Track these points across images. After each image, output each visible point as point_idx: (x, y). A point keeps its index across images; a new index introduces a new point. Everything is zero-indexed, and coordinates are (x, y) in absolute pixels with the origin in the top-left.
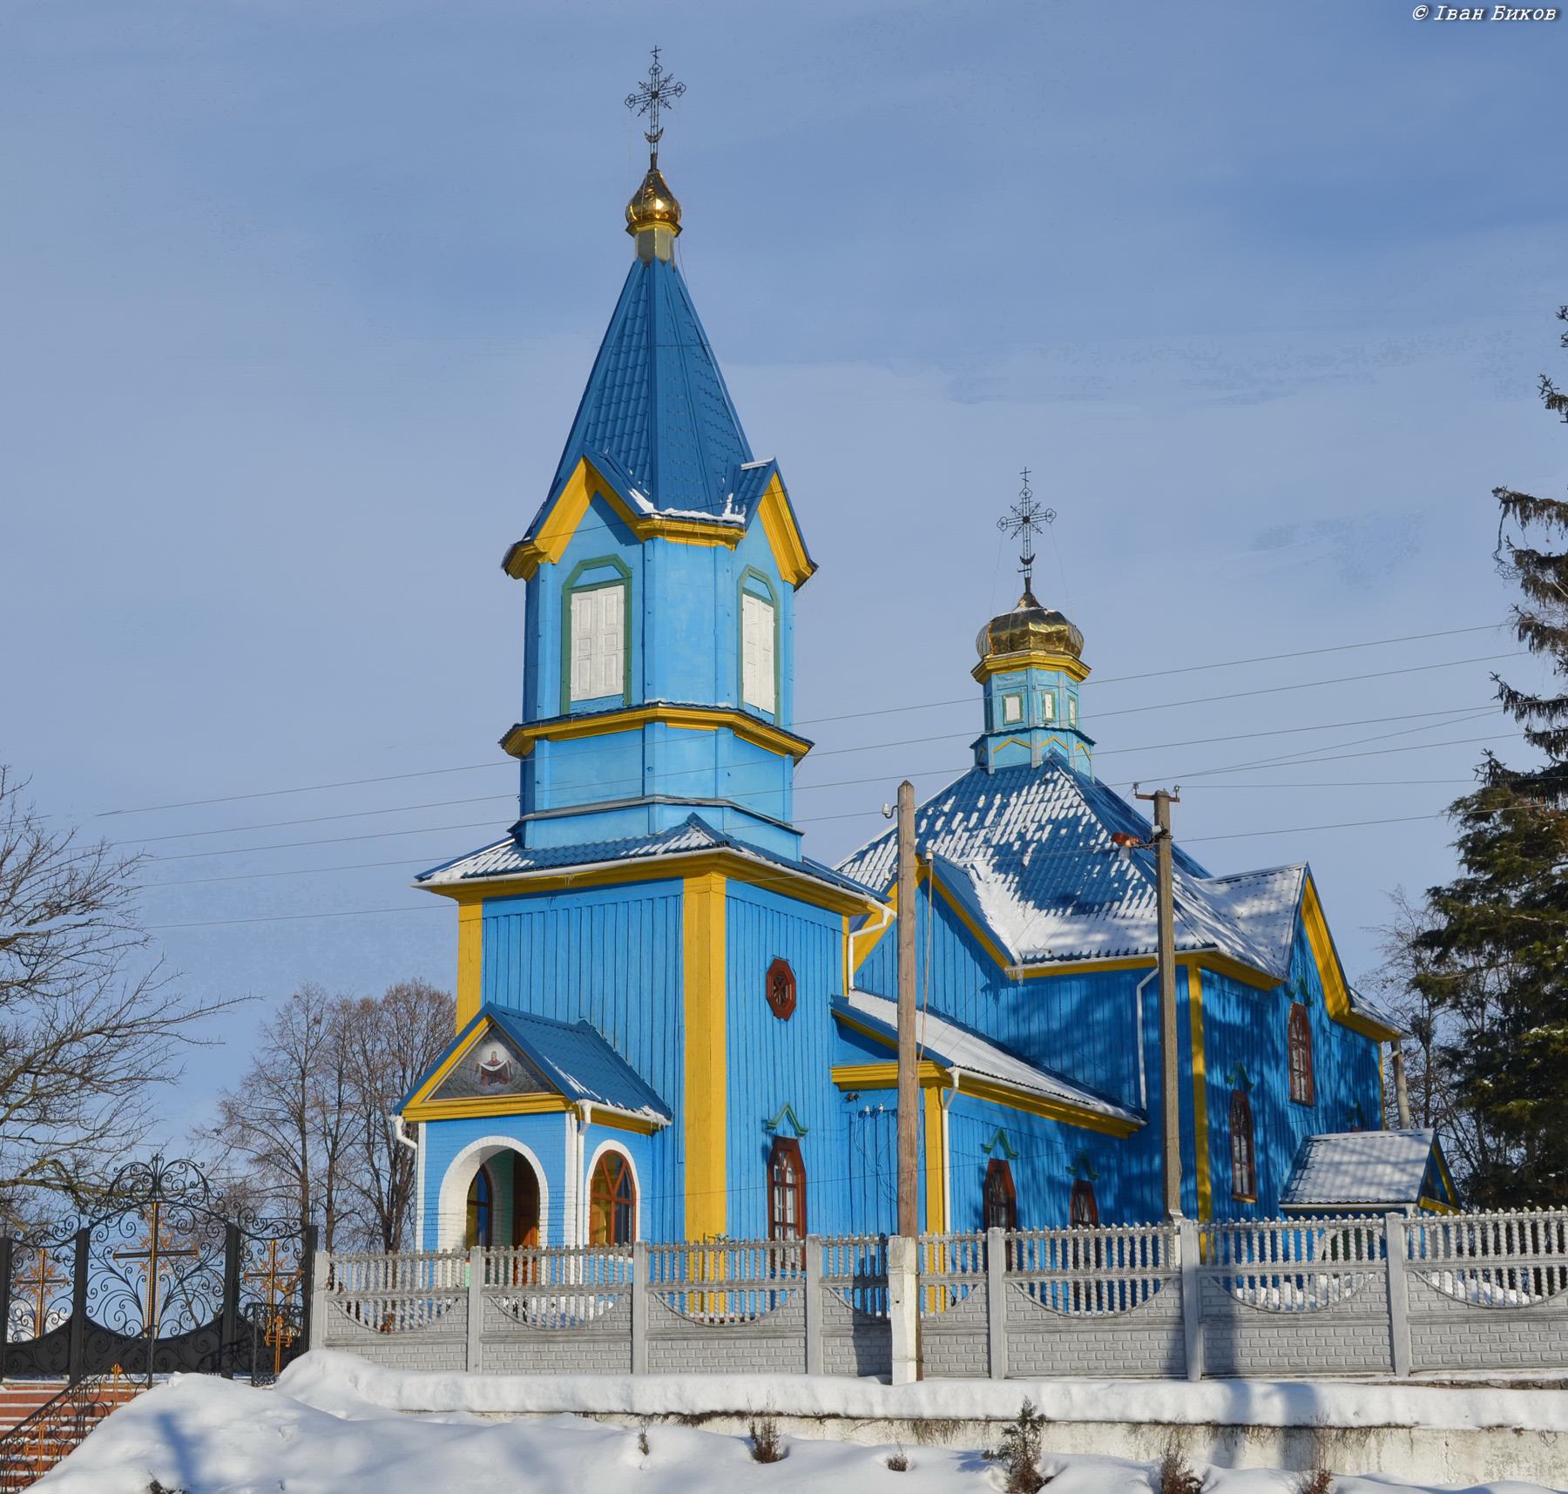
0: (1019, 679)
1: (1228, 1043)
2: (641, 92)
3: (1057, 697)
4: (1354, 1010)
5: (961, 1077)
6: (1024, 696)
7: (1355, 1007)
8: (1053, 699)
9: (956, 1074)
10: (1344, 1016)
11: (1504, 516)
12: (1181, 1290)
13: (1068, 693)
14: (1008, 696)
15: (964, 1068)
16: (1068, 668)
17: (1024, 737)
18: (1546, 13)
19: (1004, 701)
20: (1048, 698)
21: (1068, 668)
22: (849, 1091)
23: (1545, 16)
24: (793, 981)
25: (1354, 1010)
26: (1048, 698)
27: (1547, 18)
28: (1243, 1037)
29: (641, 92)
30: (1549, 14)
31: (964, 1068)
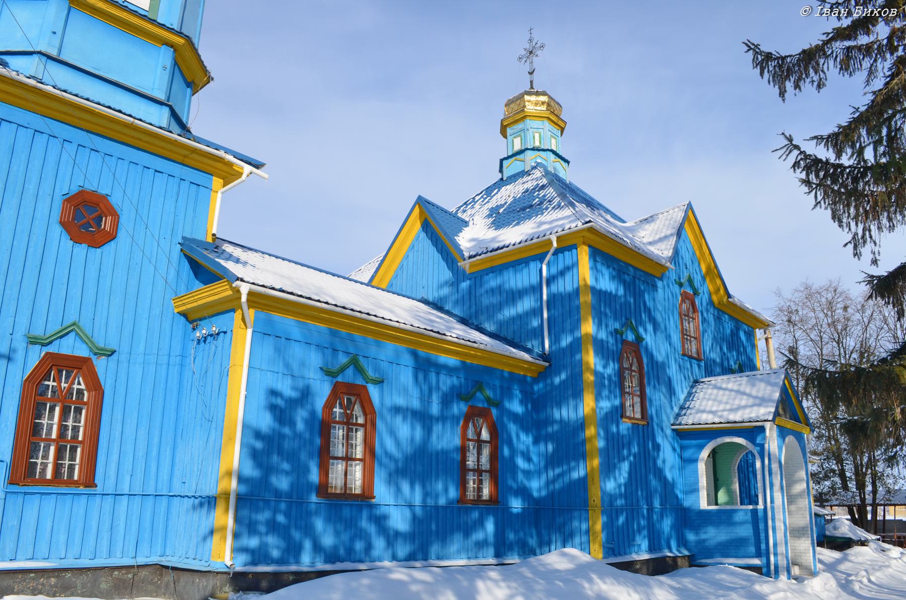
0: (520, 127)
1: (633, 306)
2: (537, 53)
3: (542, 134)
4: (730, 300)
5: (250, 294)
6: (523, 135)
7: (731, 298)
8: (540, 135)
9: (244, 289)
10: (723, 304)
11: (863, 281)
12: (300, 441)
13: (550, 133)
14: (515, 138)
15: (253, 284)
16: (548, 118)
17: (521, 157)
18: (890, 11)
19: (513, 140)
20: (537, 136)
21: (548, 118)
22: (192, 318)
23: (889, 13)
24: (64, 224)
25: (730, 300)
26: (537, 136)
27: (891, 15)
28: (726, 342)
29: (537, 53)
30: (892, 12)
31: (253, 284)
